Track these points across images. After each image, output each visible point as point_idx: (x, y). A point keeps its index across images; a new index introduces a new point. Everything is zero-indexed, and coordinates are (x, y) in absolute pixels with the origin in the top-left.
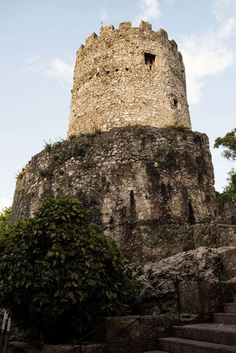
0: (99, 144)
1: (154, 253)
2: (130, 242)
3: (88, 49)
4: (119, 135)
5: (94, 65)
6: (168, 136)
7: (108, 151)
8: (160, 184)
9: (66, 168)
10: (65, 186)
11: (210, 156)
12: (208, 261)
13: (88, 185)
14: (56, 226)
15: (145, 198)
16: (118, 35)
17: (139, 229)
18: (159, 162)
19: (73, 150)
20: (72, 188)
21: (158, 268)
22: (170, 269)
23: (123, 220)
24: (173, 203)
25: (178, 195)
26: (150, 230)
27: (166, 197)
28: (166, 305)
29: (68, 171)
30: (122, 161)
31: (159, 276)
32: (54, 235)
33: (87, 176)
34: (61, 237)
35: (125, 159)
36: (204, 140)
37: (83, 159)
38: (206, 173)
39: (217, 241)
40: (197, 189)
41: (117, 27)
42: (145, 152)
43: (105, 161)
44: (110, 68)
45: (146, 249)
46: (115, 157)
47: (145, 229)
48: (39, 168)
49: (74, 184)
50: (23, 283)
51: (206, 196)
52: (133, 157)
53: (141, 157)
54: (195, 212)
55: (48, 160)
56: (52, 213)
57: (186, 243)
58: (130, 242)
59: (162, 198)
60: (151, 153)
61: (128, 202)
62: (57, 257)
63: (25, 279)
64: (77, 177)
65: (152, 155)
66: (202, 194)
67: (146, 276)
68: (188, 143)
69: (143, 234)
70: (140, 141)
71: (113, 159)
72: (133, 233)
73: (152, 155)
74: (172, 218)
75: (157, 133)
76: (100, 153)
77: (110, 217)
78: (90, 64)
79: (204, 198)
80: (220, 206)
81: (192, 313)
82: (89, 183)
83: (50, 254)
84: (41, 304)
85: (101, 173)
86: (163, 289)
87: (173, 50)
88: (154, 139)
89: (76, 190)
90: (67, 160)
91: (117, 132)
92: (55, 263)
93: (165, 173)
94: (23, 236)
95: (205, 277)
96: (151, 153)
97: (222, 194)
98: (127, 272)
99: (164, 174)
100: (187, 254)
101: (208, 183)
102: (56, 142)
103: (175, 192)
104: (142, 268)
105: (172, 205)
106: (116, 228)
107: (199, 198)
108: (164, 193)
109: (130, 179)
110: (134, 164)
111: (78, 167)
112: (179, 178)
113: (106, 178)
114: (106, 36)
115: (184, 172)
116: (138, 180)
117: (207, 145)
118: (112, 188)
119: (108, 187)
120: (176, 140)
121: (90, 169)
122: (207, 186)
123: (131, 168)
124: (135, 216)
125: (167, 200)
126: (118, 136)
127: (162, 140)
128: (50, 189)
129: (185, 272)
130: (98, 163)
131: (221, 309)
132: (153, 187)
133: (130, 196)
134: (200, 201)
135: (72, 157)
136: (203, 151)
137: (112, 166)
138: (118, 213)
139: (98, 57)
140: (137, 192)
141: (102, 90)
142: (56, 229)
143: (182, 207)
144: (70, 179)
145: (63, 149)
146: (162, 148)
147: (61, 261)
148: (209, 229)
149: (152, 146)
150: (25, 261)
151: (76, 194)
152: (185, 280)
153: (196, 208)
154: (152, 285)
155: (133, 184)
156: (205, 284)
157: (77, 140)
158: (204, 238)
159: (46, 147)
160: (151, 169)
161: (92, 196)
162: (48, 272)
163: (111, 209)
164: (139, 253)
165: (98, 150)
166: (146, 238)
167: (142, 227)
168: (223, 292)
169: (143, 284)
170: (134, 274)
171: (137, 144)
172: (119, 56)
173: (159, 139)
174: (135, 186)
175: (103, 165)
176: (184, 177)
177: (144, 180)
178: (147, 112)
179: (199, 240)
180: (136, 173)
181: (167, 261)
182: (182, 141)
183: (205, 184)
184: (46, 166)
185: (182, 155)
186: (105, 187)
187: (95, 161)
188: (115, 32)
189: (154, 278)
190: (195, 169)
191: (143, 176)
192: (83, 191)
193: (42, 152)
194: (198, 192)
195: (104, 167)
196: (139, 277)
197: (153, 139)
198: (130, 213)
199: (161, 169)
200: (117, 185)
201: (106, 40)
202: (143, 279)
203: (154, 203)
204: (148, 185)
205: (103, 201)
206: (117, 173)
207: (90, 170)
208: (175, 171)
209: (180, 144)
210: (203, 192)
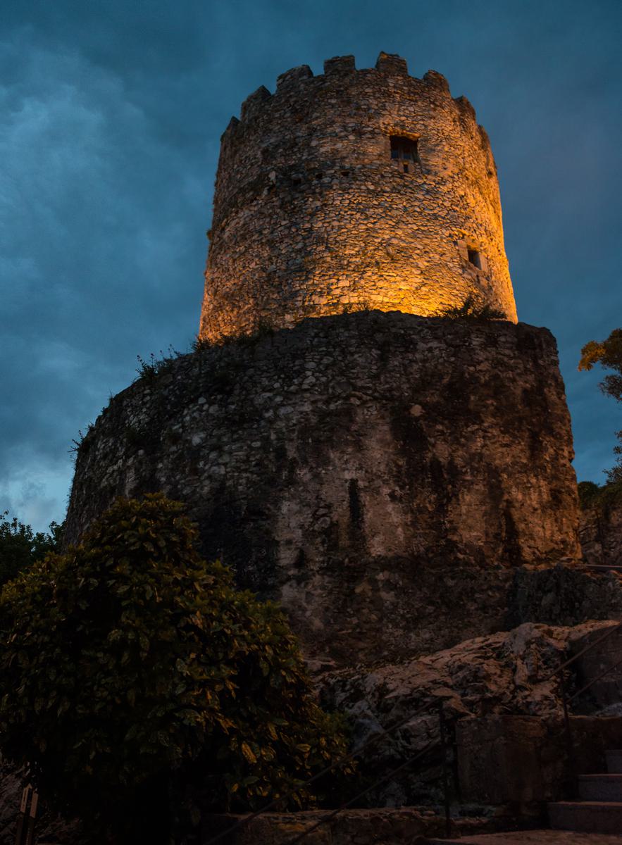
0: (269, 360)
1: (413, 644)
2: (350, 614)
3: (248, 128)
4: (320, 337)
5: (263, 166)
6: (449, 336)
7: (291, 379)
9: (186, 424)
10: (183, 472)
11: (561, 387)
12: (542, 660)
13: (242, 468)
14: (131, 567)
15: (388, 498)
17: (373, 582)
18: (424, 405)
19: (204, 380)
20: (200, 476)
21: (403, 680)
22: (434, 682)
23: (330, 558)
24: (464, 511)
25: (477, 490)
26: (401, 583)
28: (422, 782)
29: (189, 433)
30: (327, 402)
31: (403, 703)
32: (126, 588)
33: (238, 445)
34: (142, 595)
35: (335, 400)
36: (544, 346)
37: (229, 401)
38: (551, 432)
39: (578, 608)
40: (526, 472)
41: (318, 70)
42: (389, 380)
43: (284, 405)
44: (301, 170)
45: (391, 634)
46: (308, 395)
47: (388, 580)
48: (127, 425)
49: (205, 465)
50: (50, 704)
51: (551, 490)
52: (357, 393)
53: (378, 392)
54: (521, 534)
55: (148, 405)
56: (122, 537)
57: (497, 615)
58: (350, 616)
59: (433, 497)
60: (404, 383)
61: (344, 510)
62: (129, 642)
63: (54, 693)
64: (213, 448)
65: (405, 386)
66: (539, 487)
67: (371, 702)
68: (502, 355)
69: (383, 594)
70: (373, 350)
71: (305, 400)
72: (358, 590)
73: (405, 386)
74: (460, 551)
75: (420, 328)
76: (272, 386)
77: (296, 549)
78: (252, 165)
79: (545, 496)
80: (598, 519)
81: (490, 804)
82: (244, 462)
83: (115, 634)
84: (91, 757)
85: (273, 437)
86: (415, 736)
87: (463, 121)
88: (411, 346)
89: (211, 481)
90: (188, 404)
91: (316, 331)
92: (126, 657)
93: (442, 433)
94: (54, 591)
95: (529, 703)
96: (404, 383)
97: (604, 488)
98: (322, 692)
99: (439, 435)
100: (489, 642)
101: (555, 458)
102: (162, 359)
103: (468, 481)
104: (360, 681)
105: (461, 515)
106: (312, 579)
107: (533, 497)
108: (437, 486)
109: (350, 450)
110: (359, 411)
111: (214, 422)
112: (479, 444)
113: (286, 450)
115: (490, 430)
116: (371, 452)
117: (552, 358)
118: (302, 473)
119: (292, 471)
120: (469, 345)
121: (245, 426)
122: (552, 465)
123: (352, 421)
124: (364, 546)
126: (316, 340)
127: (431, 347)
128: (152, 476)
129: (477, 690)
130: (267, 410)
131: (570, 789)
133: (348, 496)
134: (534, 503)
135: (200, 396)
136: (542, 374)
137: (302, 418)
138: (319, 540)
139: (272, 146)
140: (367, 484)
141: (282, 228)
142: (131, 574)
143: (486, 521)
144: (196, 454)
145: (179, 377)
146: (432, 368)
147: (141, 653)
148: (555, 578)
149: (407, 362)
150: (58, 650)
151: (210, 492)
152: (476, 713)
153: (526, 523)
155: (357, 462)
156: (524, 722)
157: (214, 354)
158: (543, 602)
159: (142, 374)
160: (403, 424)
161: (250, 497)
162: (109, 680)
163: (301, 528)
164: (374, 642)
165: (267, 377)
166: (392, 604)
167: (381, 576)
168: (576, 745)
169: (362, 724)
170: (340, 696)
171: (367, 358)
173: (425, 346)
174: (361, 468)
175: (278, 416)
176: (493, 441)
177: (386, 452)
179: (530, 607)
180: (366, 435)
181: (430, 663)
182: (485, 349)
183: (548, 459)
184: (143, 419)
185: (486, 385)
186: (285, 473)
187: (260, 405)
188: (315, 82)
189: (392, 708)
190: (520, 419)
191: (381, 441)
192: (229, 483)
193: (133, 385)
194: (528, 482)
195: (281, 420)
196: (353, 706)
197: (408, 345)
198: (350, 539)
199: (429, 422)
200: (314, 466)
201: (292, 104)
202: (363, 711)
203: (412, 511)
204: (397, 465)
205: (279, 509)
206: (314, 434)
207: (245, 428)
208: (468, 426)
209: (481, 356)
210: (544, 480)
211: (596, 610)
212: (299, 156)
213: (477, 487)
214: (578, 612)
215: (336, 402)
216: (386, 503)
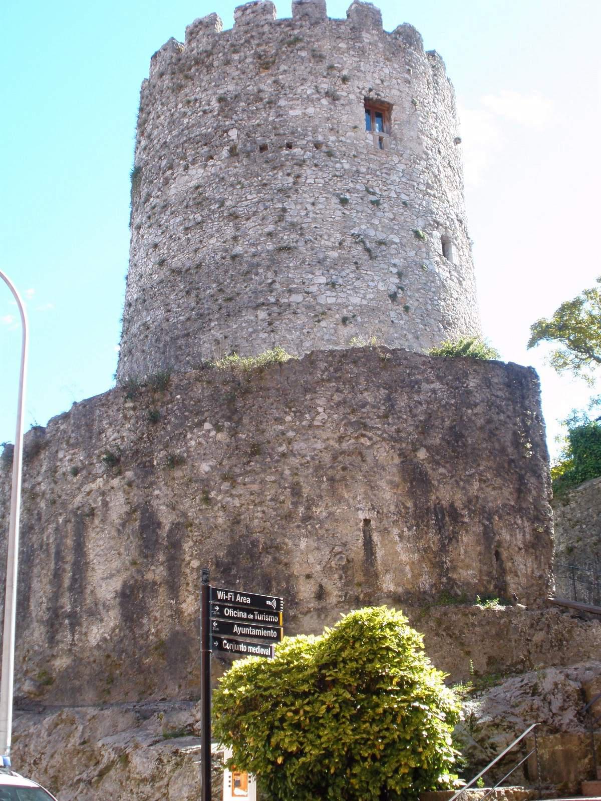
7: (302, 414)
8: (431, 504)
15: (397, 538)
16: (290, 35)
18: (428, 448)
27: (446, 537)
31: (488, 726)
79: (528, 536)
85: (287, 472)
107: (518, 536)
112: (476, 488)
113: (301, 486)
114: (254, 34)
118: (318, 511)
125: (448, 544)
126: (326, 373)
132: (415, 511)
141: (248, 202)
145: (179, 397)
154: (477, 742)
163: (319, 564)
172: (295, 102)
174: (373, 509)
178: (376, 278)
185: (481, 428)
186: (301, 510)
188: (283, 26)
191: (391, 482)
194: (515, 523)
198: (364, 575)
204: (406, 507)
211: (580, 648)
212: (265, 115)
213: (474, 529)
214: (565, 648)
215: (348, 441)
216: (396, 543)
